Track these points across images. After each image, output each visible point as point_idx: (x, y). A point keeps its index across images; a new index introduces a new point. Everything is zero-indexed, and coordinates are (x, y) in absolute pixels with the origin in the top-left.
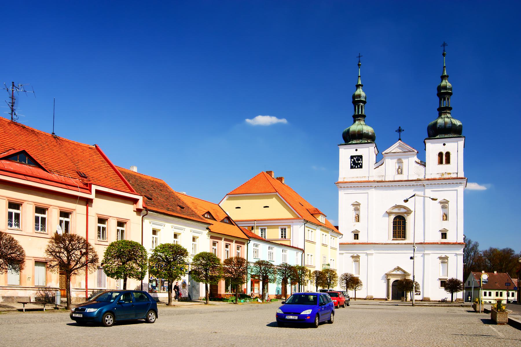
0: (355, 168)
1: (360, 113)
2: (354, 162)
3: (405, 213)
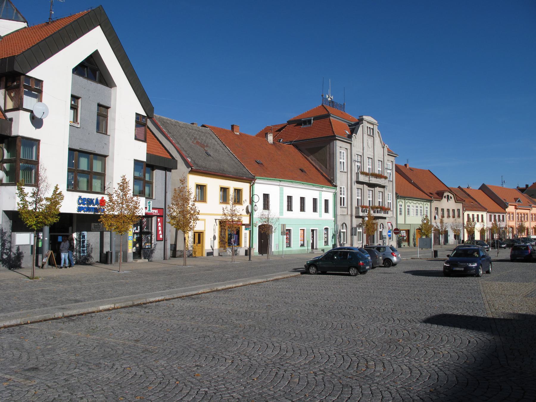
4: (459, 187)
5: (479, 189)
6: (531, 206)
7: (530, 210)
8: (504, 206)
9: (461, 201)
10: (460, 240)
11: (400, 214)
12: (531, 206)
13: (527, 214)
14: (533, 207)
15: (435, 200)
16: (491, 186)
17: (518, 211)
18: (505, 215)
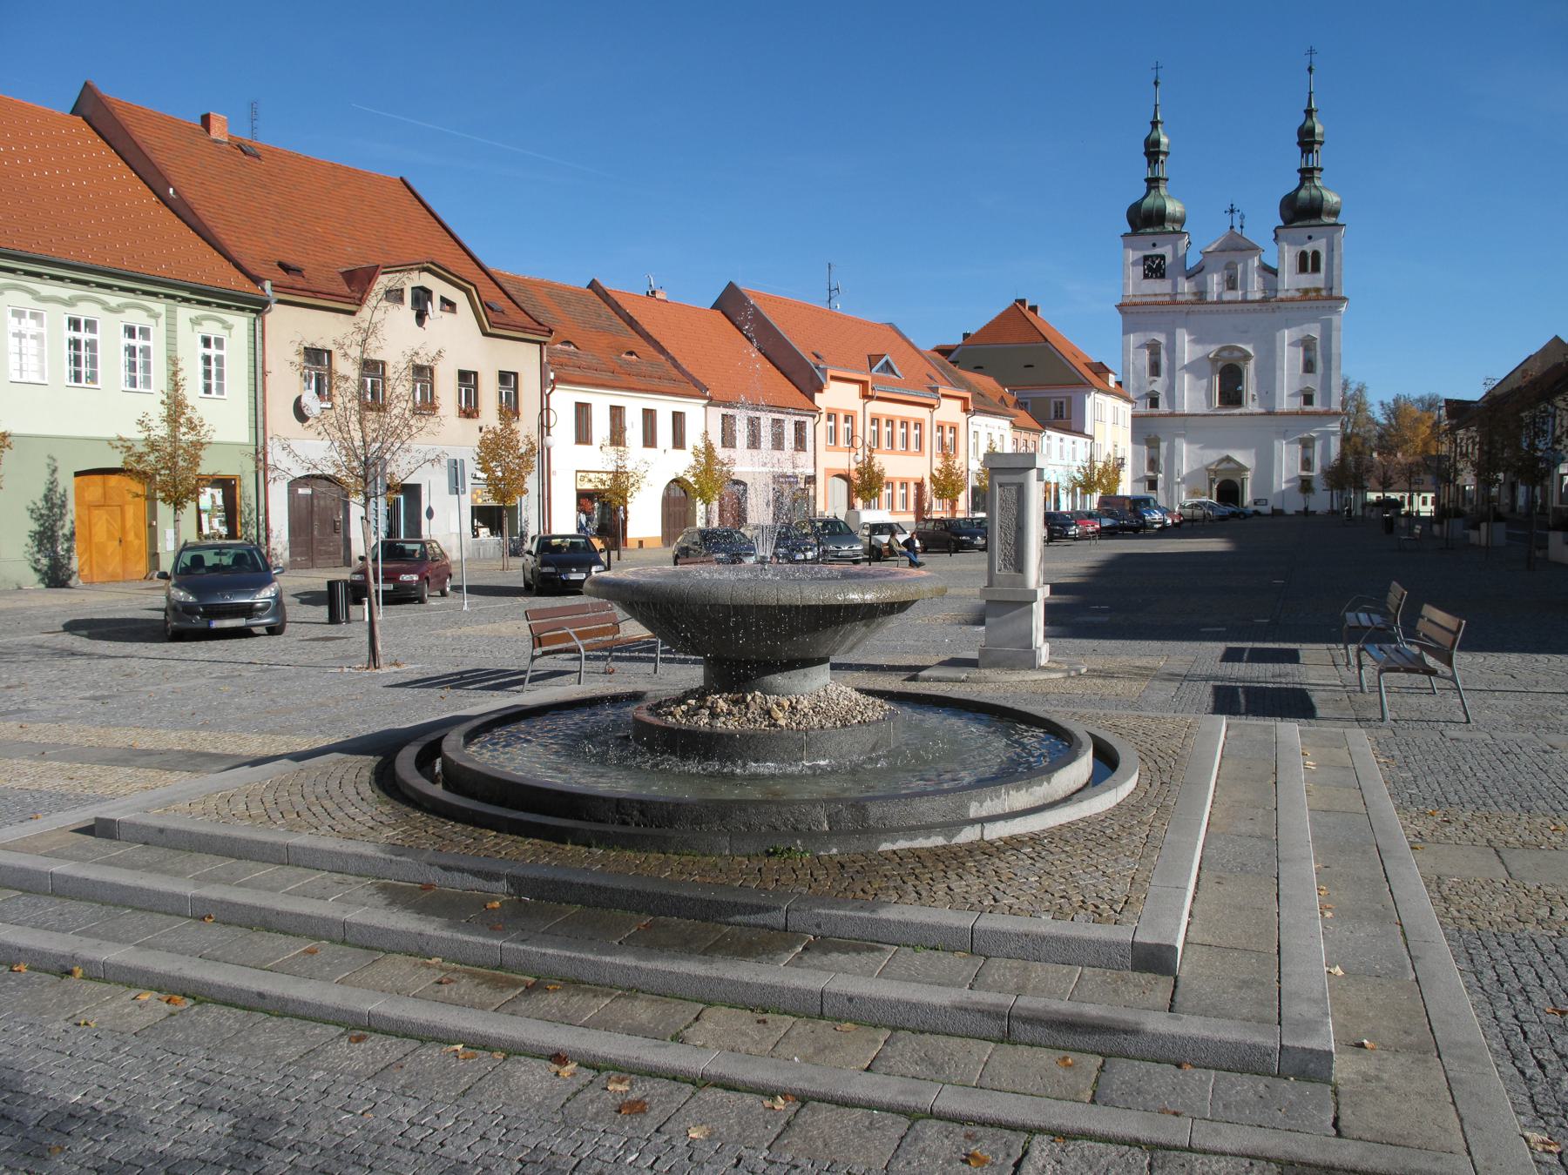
0: (1152, 277)
4: (593, 285)
5: (715, 307)
6: (935, 390)
7: (931, 406)
8: (808, 382)
9: (524, 329)
10: (523, 535)
11: (207, 389)
12: (935, 390)
13: (919, 425)
14: (944, 396)
15: (280, 302)
16: (758, 296)
17: (876, 407)
18: (809, 422)
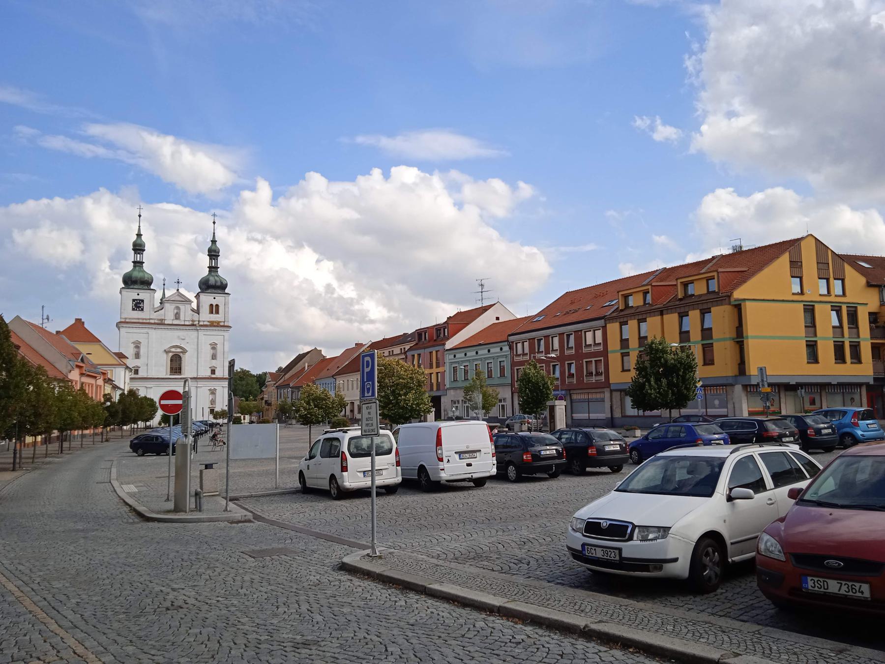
1: (213, 265)
2: (136, 305)
3: (181, 352)
